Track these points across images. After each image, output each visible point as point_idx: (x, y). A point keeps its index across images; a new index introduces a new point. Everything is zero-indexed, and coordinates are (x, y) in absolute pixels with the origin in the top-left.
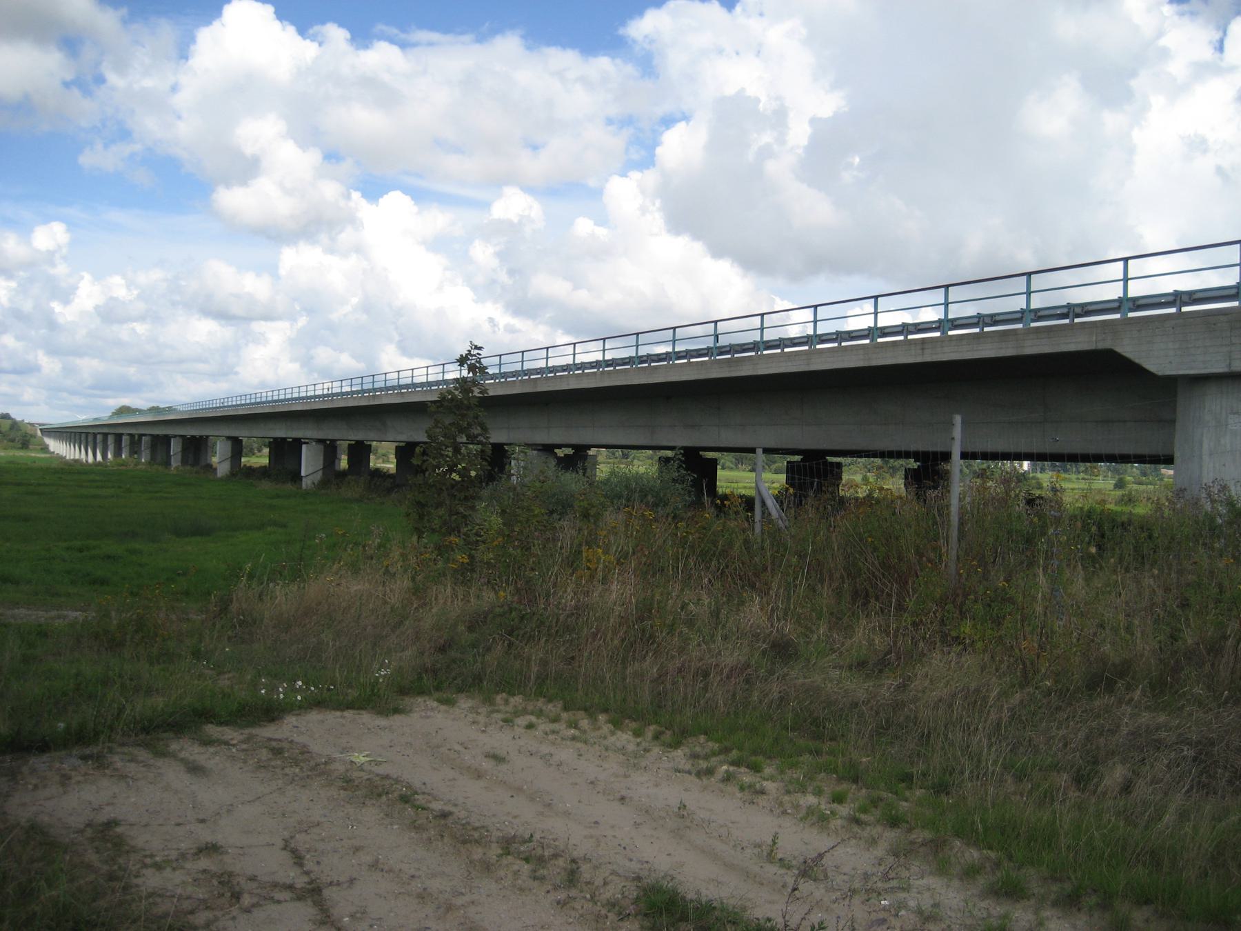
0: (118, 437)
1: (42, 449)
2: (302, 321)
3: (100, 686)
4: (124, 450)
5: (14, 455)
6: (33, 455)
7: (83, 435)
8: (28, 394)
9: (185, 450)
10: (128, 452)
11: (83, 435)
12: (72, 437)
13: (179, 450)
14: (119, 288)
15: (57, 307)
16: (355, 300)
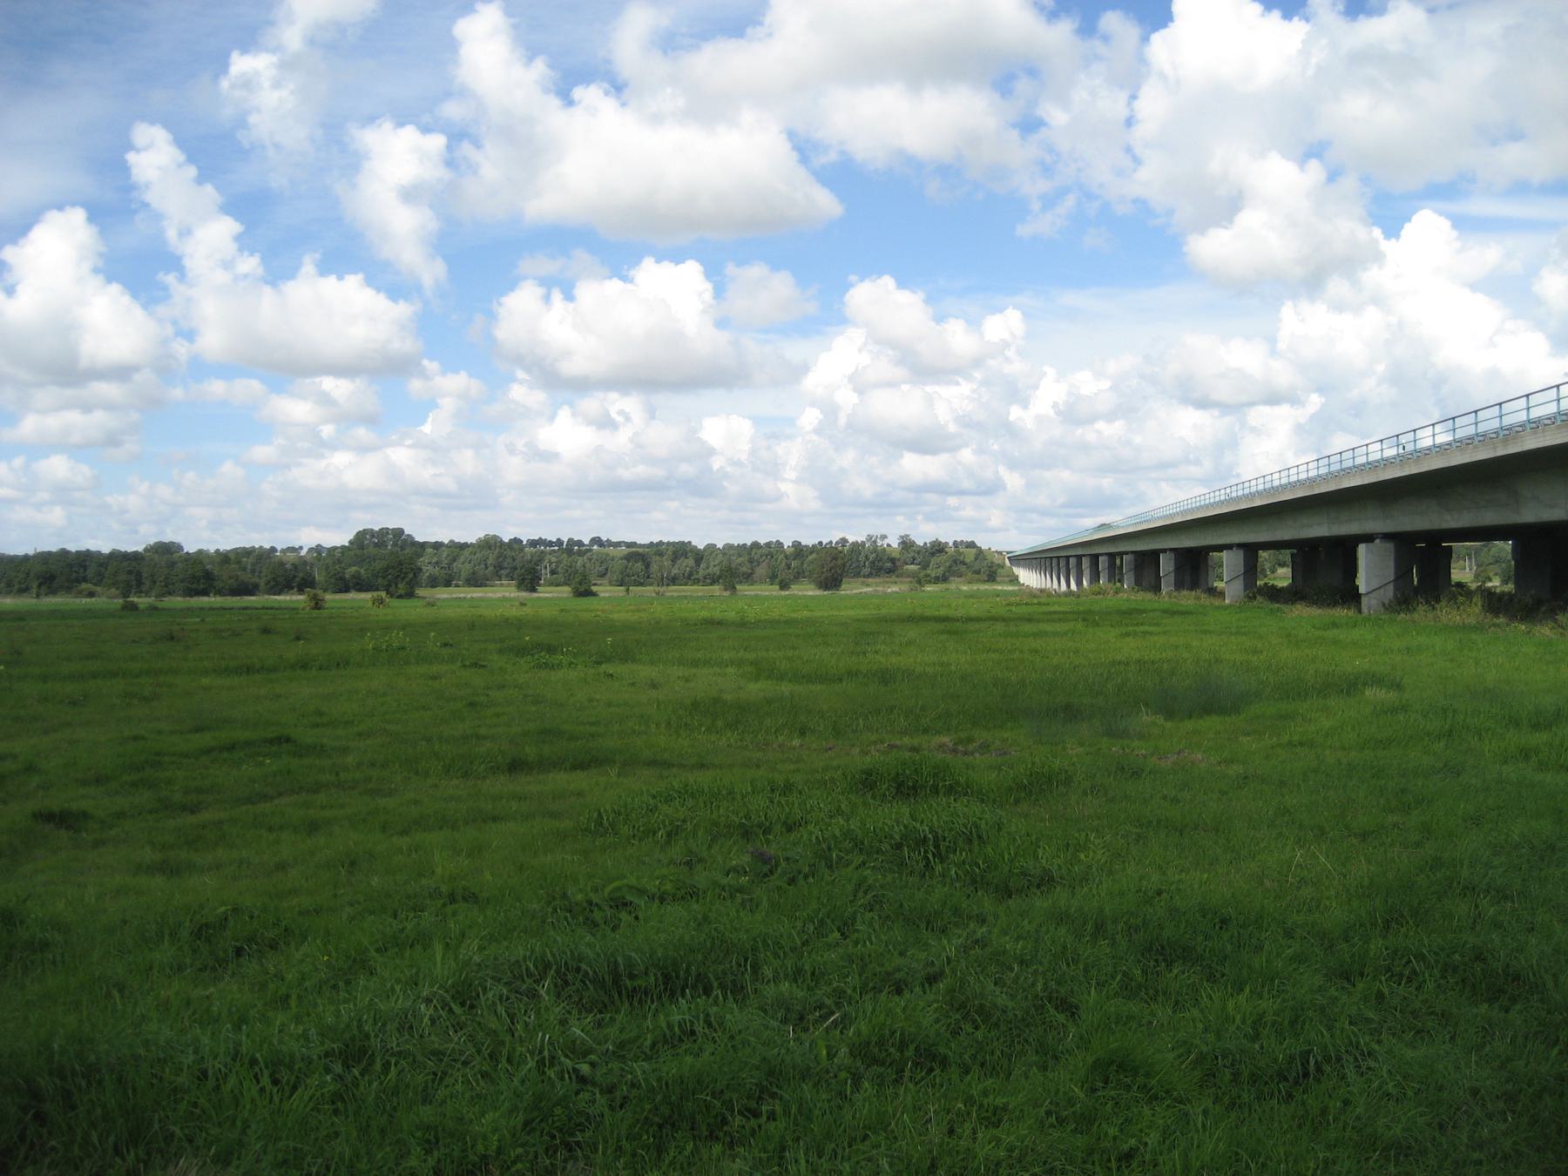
0: (1095, 558)
1: (1010, 581)
2: (1315, 401)
3: (493, 846)
4: (1085, 572)
5: (978, 589)
6: (1000, 588)
7: (1054, 561)
8: (996, 519)
9: (1178, 569)
10: (1107, 576)
11: (1054, 561)
12: (1043, 563)
13: (1172, 569)
14: (1089, 384)
15: (1015, 413)
16: (1381, 368)
